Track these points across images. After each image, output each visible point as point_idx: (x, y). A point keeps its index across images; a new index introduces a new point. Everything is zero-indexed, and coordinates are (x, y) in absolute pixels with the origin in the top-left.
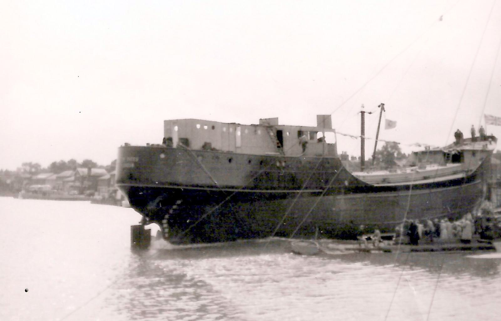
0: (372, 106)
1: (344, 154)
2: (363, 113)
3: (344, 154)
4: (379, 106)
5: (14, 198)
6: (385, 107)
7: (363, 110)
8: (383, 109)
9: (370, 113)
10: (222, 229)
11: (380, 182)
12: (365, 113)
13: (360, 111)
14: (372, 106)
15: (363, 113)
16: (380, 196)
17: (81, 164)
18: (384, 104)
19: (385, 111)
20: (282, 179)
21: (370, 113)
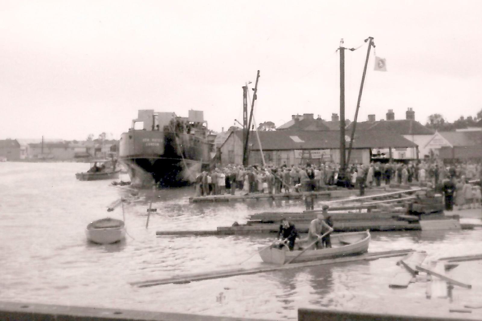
0: (355, 40)
1: (410, 110)
2: (342, 50)
3: (410, 110)
4: (366, 41)
5: (455, 121)
6: (374, 41)
7: (343, 46)
8: (372, 44)
9: (352, 50)
10: (440, 163)
11: (320, 196)
12: (345, 50)
13: (339, 47)
14: (355, 40)
15: (342, 50)
16: (376, 202)
17: (164, 154)
18: (373, 38)
19: (374, 47)
20: (319, 161)
21: (352, 50)
